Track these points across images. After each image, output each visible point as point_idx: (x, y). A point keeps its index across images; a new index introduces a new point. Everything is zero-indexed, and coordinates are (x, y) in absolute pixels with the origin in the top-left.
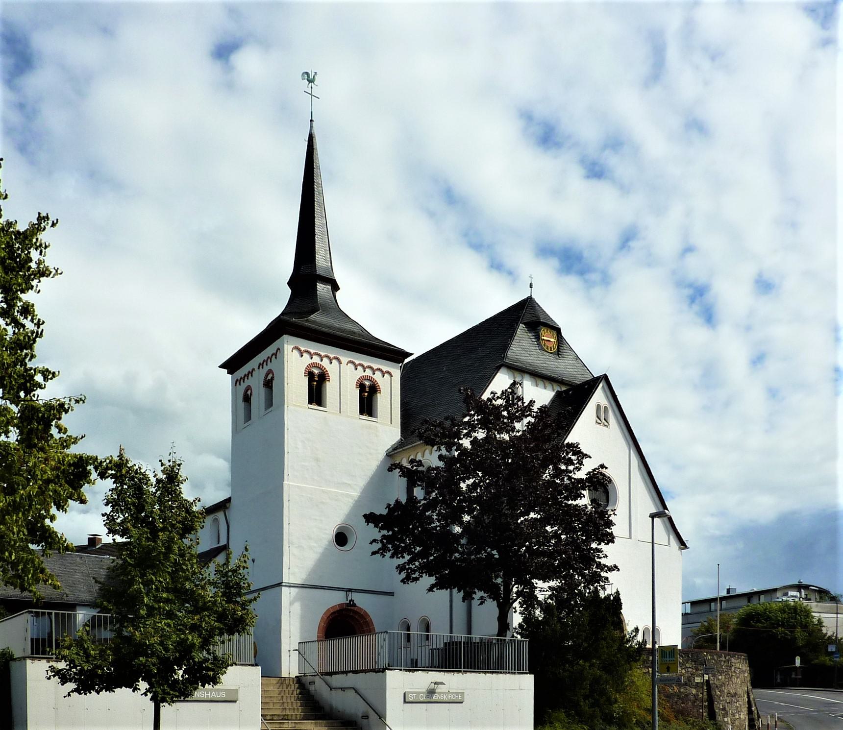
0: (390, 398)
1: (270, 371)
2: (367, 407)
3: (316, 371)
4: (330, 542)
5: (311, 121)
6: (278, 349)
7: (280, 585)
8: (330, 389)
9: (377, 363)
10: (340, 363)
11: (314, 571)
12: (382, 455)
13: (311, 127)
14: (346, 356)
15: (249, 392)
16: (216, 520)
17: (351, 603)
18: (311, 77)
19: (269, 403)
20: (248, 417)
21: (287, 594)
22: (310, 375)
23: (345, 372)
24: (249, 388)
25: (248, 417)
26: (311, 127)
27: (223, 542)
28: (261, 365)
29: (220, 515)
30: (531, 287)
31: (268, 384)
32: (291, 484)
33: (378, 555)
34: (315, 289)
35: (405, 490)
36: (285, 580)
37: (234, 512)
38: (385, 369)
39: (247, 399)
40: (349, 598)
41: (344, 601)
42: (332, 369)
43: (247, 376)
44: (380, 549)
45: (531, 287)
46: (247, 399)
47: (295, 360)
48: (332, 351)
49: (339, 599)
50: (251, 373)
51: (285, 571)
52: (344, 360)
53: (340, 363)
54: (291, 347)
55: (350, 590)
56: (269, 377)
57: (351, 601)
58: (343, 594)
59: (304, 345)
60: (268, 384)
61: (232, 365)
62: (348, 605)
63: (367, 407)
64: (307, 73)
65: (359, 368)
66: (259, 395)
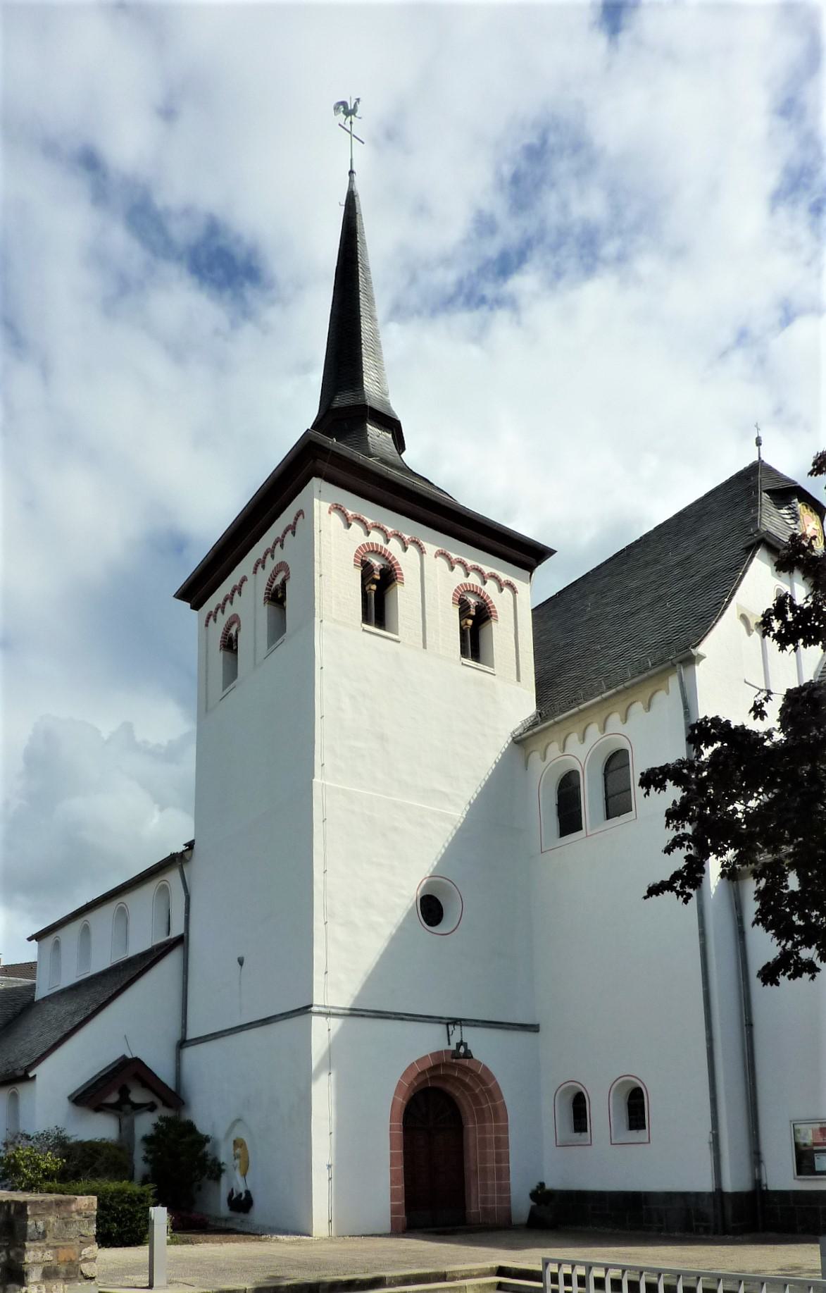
0: (512, 634)
1: (283, 567)
2: (473, 641)
3: (377, 563)
4: (409, 914)
5: (351, 172)
6: (300, 513)
7: (306, 1010)
8: (404, 598)
9: (490, 565)
10: (422, 551)
11: (375, 979)
12: (504, 741)
13: (351, 181)
14: (433, 543)
15: (233, 631)
16: (164, 890)
17: (462, 1054)
18: (351, 107)
19: (278, 628)
20: (231, 673)
21: (322, 1032)
22: (366, 568)
23: (432, 576)
24: (235, 620)
25: (231, 673)
26: (351, 181)
27: (177, 931)
28: (261, 563)
29: (173, 878)
30: (759, 443)
31: (276, 598)
32: (328, 784)
33: (669, 896)
34: (365, 429)
35: (554, 809)
36: (319, 999)
37: (196, 869)
38: (504, 577)
39: (230, 644)
40: (455, 1039)
41: (442, 1045)
42: (406, 561)
43: (229, 598)
44: (676, 876)
45: (759, 443)
46: (230, 644)
47: (335, 533)
48: (410, 528)
49: (427, 1042)
50: (238, 589)
51: (318, 977)
52: (431, 549)
53: (422, 551)
54: (326, 506)
55: (455, 1022)
56: (278, 581)
57: (459, 1045)
58: (440, 1029)
59: (355, 505)
60: (276, 598)
61: (196, 590)
62: (455, 1054)
63: (473, 641)
64: (344, 104)
65: (458, 568)
66: (252, 636)
